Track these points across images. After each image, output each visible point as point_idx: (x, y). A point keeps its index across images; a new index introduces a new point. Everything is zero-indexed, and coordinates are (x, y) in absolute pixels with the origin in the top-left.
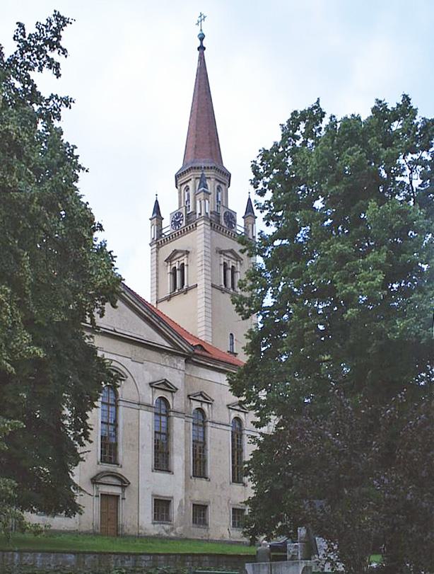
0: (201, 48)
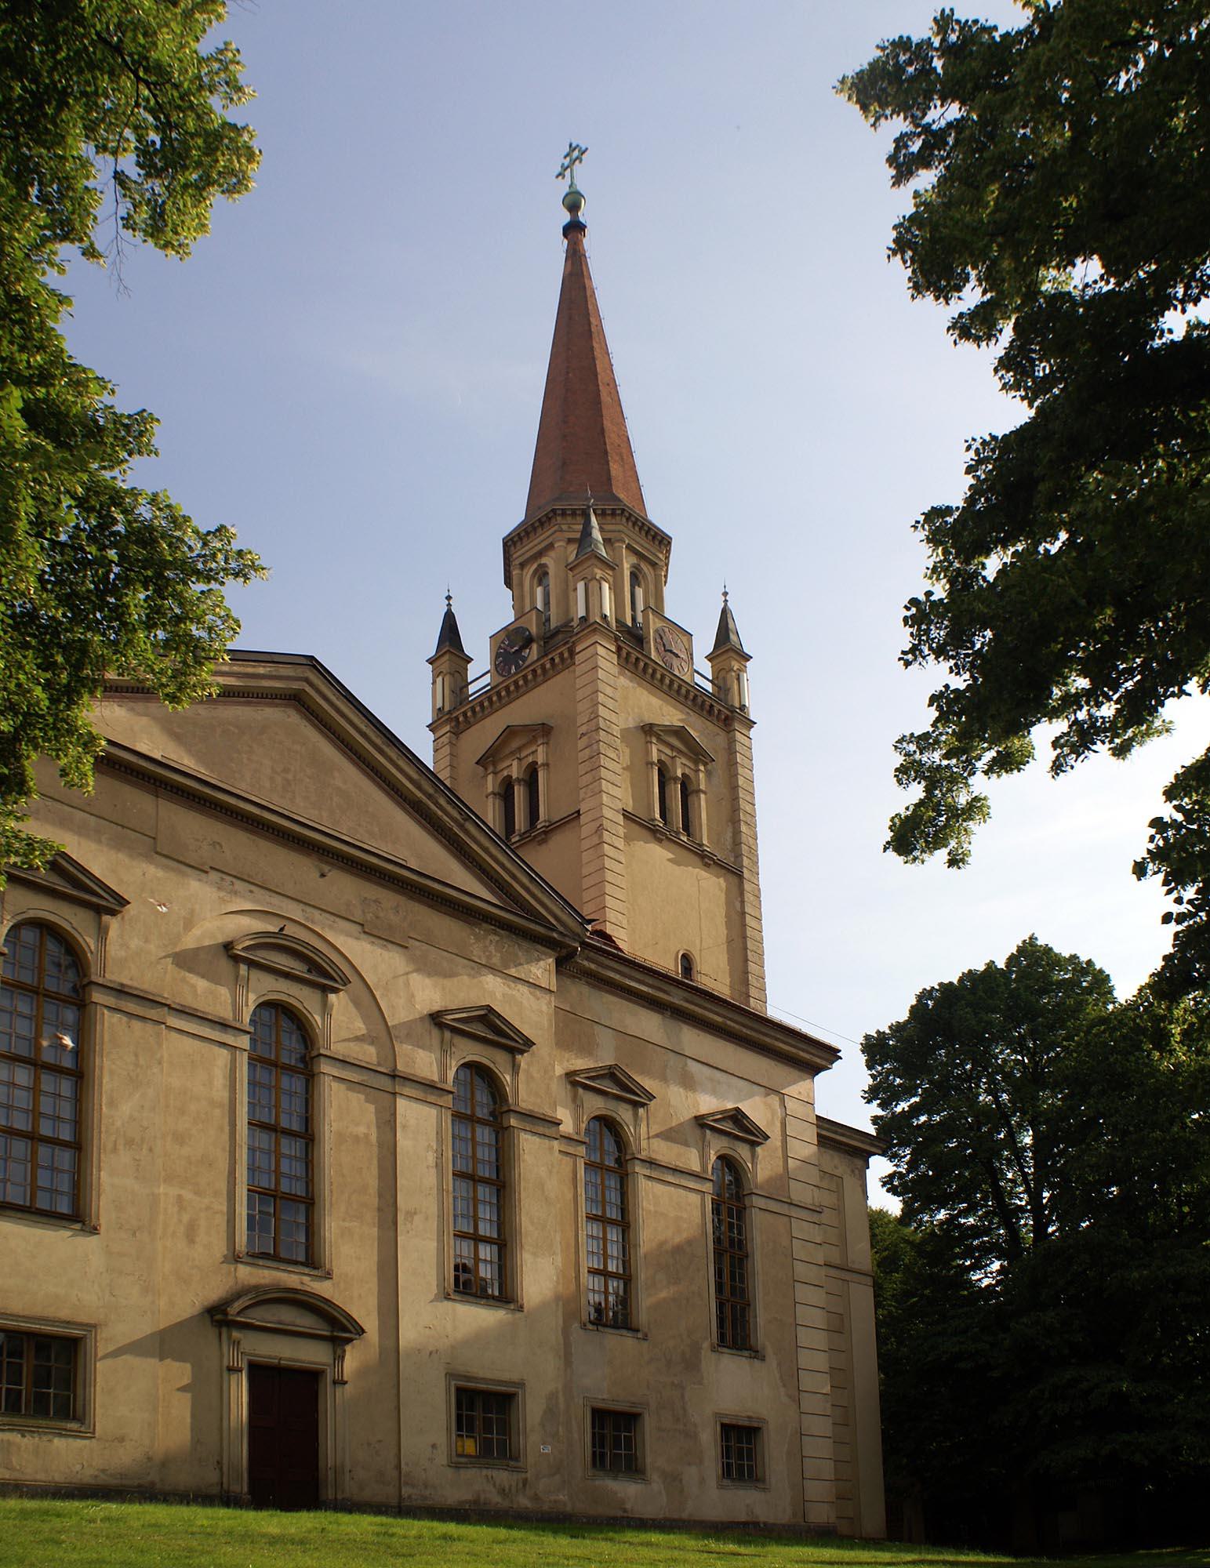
0: (574, 230)
